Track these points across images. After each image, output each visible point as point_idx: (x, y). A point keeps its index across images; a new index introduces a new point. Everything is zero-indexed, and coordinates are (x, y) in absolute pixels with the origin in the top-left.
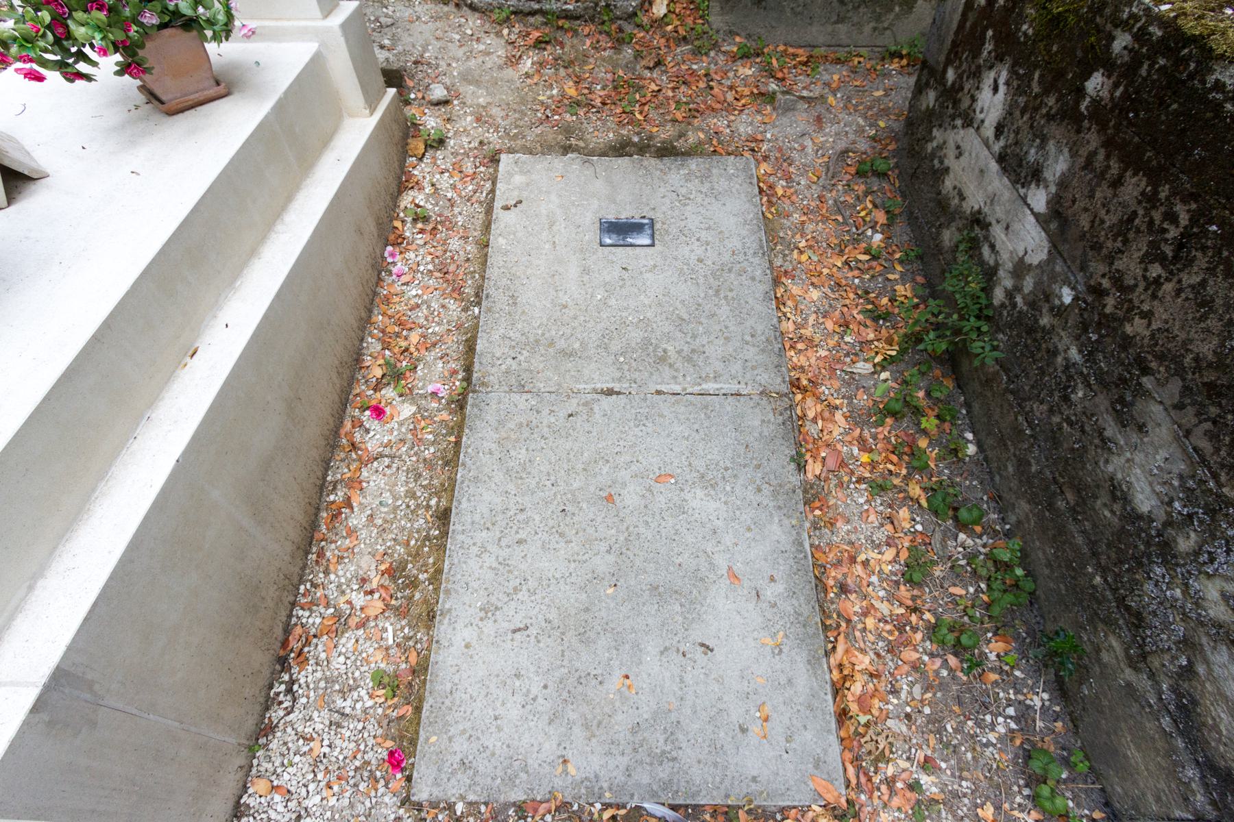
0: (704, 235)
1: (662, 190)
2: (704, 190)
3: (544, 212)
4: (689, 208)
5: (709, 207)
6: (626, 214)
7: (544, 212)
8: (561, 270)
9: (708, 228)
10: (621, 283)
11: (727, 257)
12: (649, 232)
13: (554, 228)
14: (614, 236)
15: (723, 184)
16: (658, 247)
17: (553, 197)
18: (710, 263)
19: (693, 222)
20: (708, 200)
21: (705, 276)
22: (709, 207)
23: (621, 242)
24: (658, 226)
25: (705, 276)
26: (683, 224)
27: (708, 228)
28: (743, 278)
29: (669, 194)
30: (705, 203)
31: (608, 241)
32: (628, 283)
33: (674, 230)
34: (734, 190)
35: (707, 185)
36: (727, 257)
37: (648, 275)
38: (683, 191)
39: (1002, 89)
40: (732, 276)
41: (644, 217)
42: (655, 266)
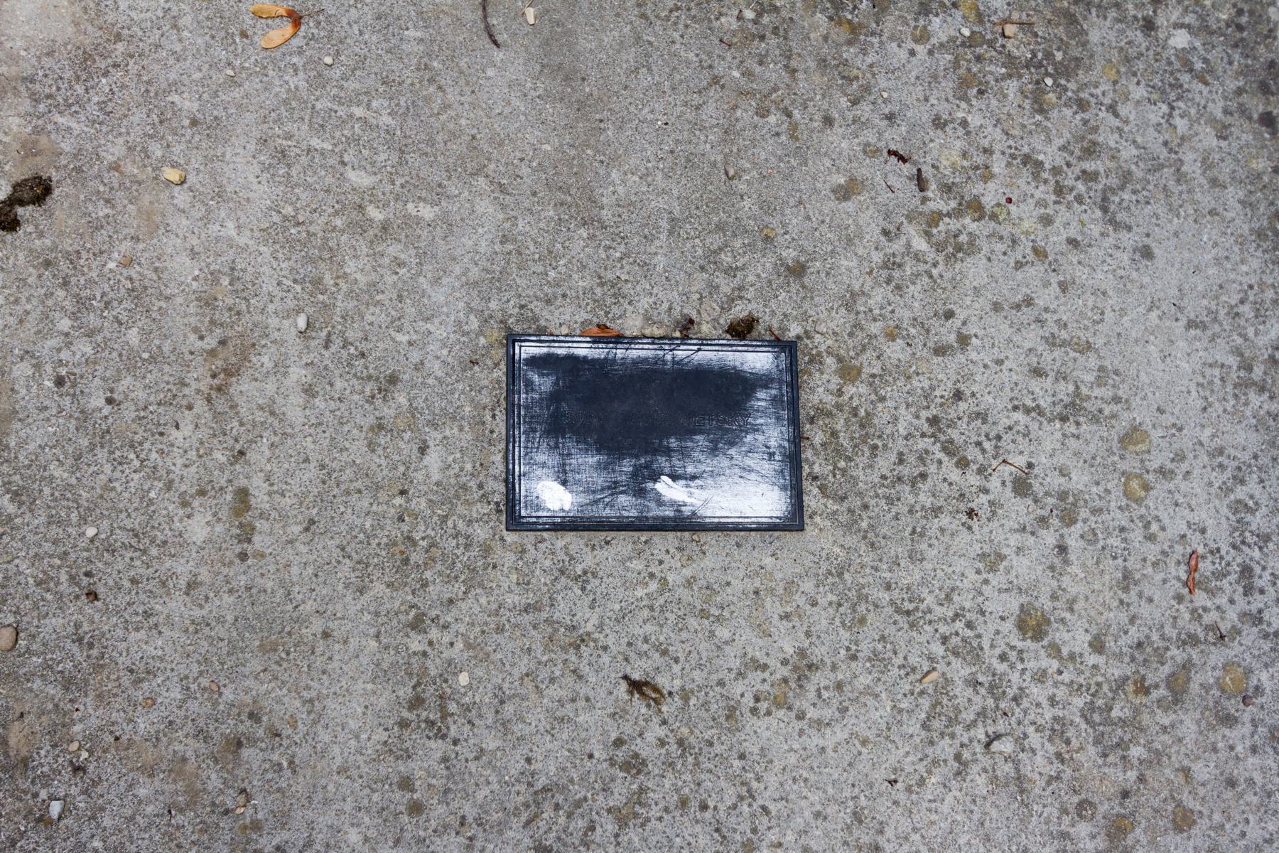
0: (1047, 448)
1: (840, 141)
2: (1049, 155)
3: (184, 269)
4: (974, 270)
5: (1072, 266)
6: (650, 305)
7: (184, 269)
8: (284, 704)
9: (1070, 411)
10: (622, 789)
11: (1159, 605)
12: (774, 435)
13: (243, 387)
14: (586, 462)
15: (1136, 123)
16: (821, 536)
17: (241, 166)
18: (1076, 639)
19: (997, 368)
20: (1067, 222)
21: (1058, 730)
22: (1072, 266)
23: (626, 506)
24: (820, 388)
25: (1058, 730)
26: (945, 373)
27: (1070, 411)
28: (1239, 735)
29: (868, 170)
30: (1056, 239)
31: (552, 496)
32: (663, 789)
33: (900, 419)
34: (1191, 164)
35: (1065, 120)
36: (1159, 605)
37: (765, 731)
38: (945, 153)
39: (598, 352)
40: (1189, 723)
41: (742, 331)
42: (804, 666)
